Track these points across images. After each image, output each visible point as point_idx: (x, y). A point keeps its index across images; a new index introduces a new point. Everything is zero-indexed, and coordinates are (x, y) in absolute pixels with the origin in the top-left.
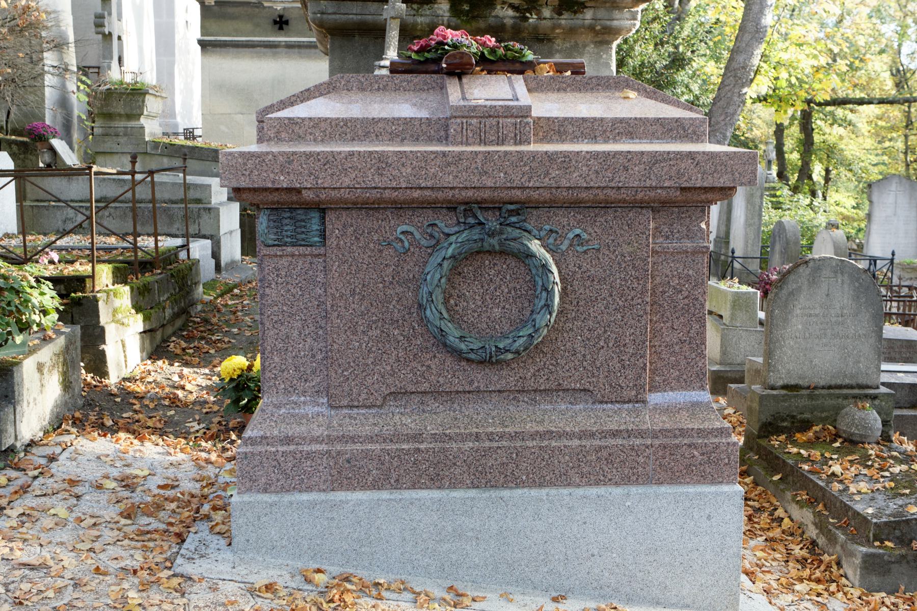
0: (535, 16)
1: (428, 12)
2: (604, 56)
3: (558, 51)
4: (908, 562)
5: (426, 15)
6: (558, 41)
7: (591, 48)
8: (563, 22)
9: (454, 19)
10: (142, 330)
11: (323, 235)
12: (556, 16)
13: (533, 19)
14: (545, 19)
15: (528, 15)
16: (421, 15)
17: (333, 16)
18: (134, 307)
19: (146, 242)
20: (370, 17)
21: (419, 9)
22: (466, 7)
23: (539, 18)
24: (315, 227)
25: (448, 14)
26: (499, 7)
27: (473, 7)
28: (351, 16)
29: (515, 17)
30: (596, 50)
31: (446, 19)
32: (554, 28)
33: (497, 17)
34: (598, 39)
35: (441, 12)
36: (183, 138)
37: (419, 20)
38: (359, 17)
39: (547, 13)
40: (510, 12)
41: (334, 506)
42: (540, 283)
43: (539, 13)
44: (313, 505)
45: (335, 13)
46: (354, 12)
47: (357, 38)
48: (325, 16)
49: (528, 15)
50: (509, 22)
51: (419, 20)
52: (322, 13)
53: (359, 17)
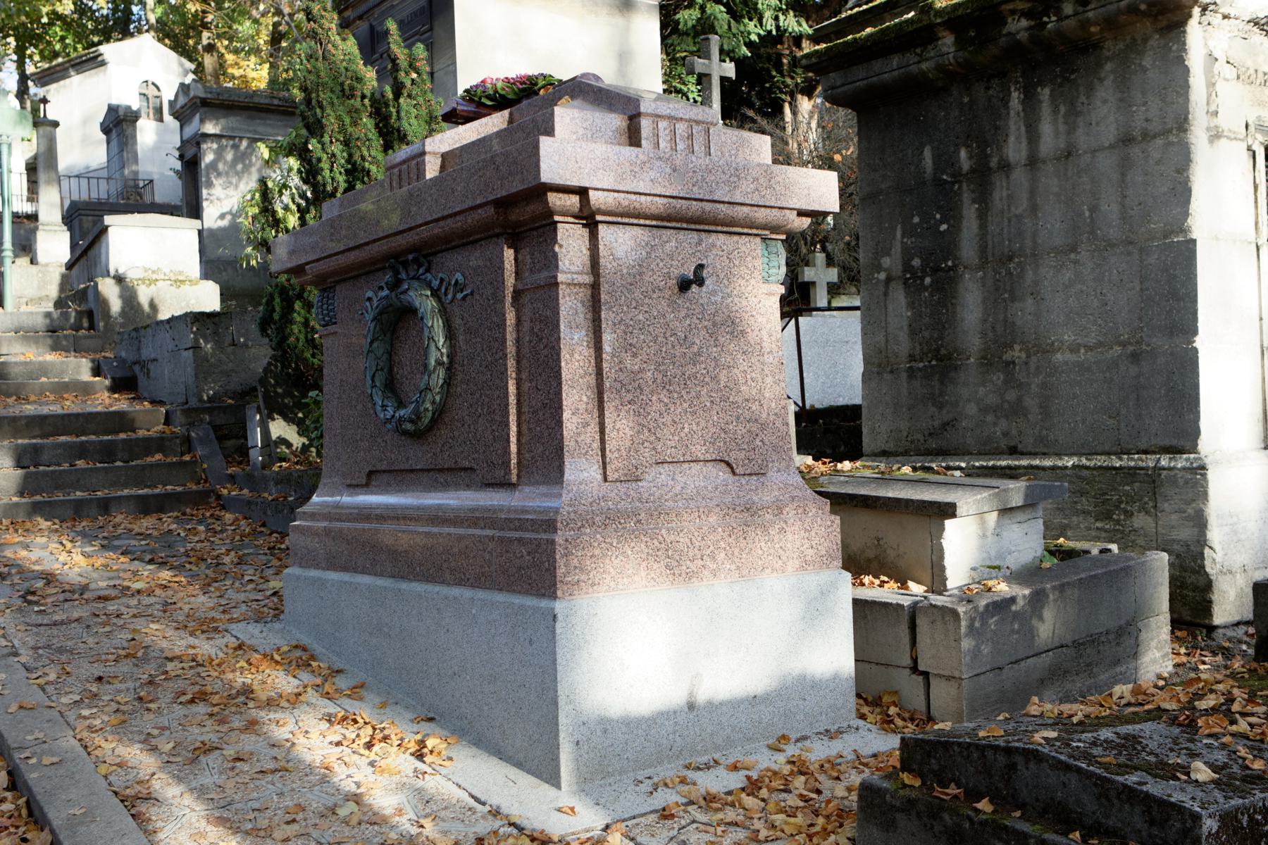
0: (1054, 18)
2: (1175, 48)
3: (1108, 59)
4: (918, 815)
5: (932, 58)
6: (1108, 44)
7: (1155, 41)
8: (1090, 14)
10: (949, 523)
12: (1081, 9)
13: (1051, 23)
14: (1067, 17)
15: (1045, 19)
17: (845, 88)
18: (102, 124)
19: (1164, 462)
23: (1060, 19)
26: (1010, 20)
29: (1030, 28)
30: (1162, 42)
31: (951, 56)
32: (1084, 25)
33: (1009, 34)
34: (1164, 23)
35: (945, 49)
39: (1068, 9)
40: (1024, 23)
43: (1058, 12)
45: (843, 85)
49: (1045, 19)
50: (1023, 36)
51: (924, 66)
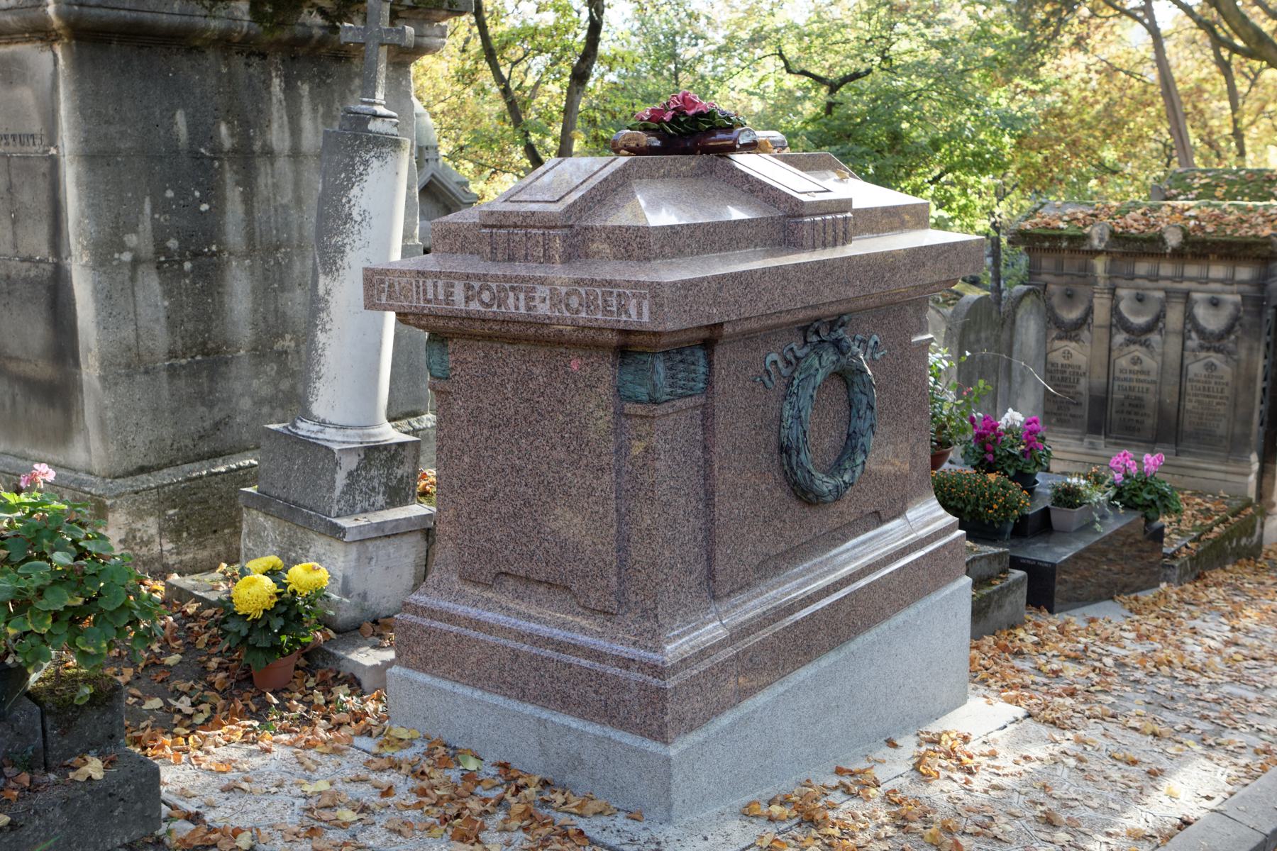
1: (223, 13)
9: (256, 26)
11: (709, 382)
16: (214, 17)
20: (148, 15)
21: (212, 6)
22: (268, 9)
24: (702, 370)
25: (247, 18)
26: (305, 11)
27: (277, 7)
28: (123, 13)
29: (323, 27)
33: (303, 25)
36: (1196, 296)
37: (214, 24)
38: (134, 15)
40: (319, 20)
41: (747, 719)
42: (865, 401)
44: (426, 687)
46: (127, 6)
47: (114, 45)
48: (85, 10)
50: (317, 33)
52: (81, 5)
53: (134, 15)
